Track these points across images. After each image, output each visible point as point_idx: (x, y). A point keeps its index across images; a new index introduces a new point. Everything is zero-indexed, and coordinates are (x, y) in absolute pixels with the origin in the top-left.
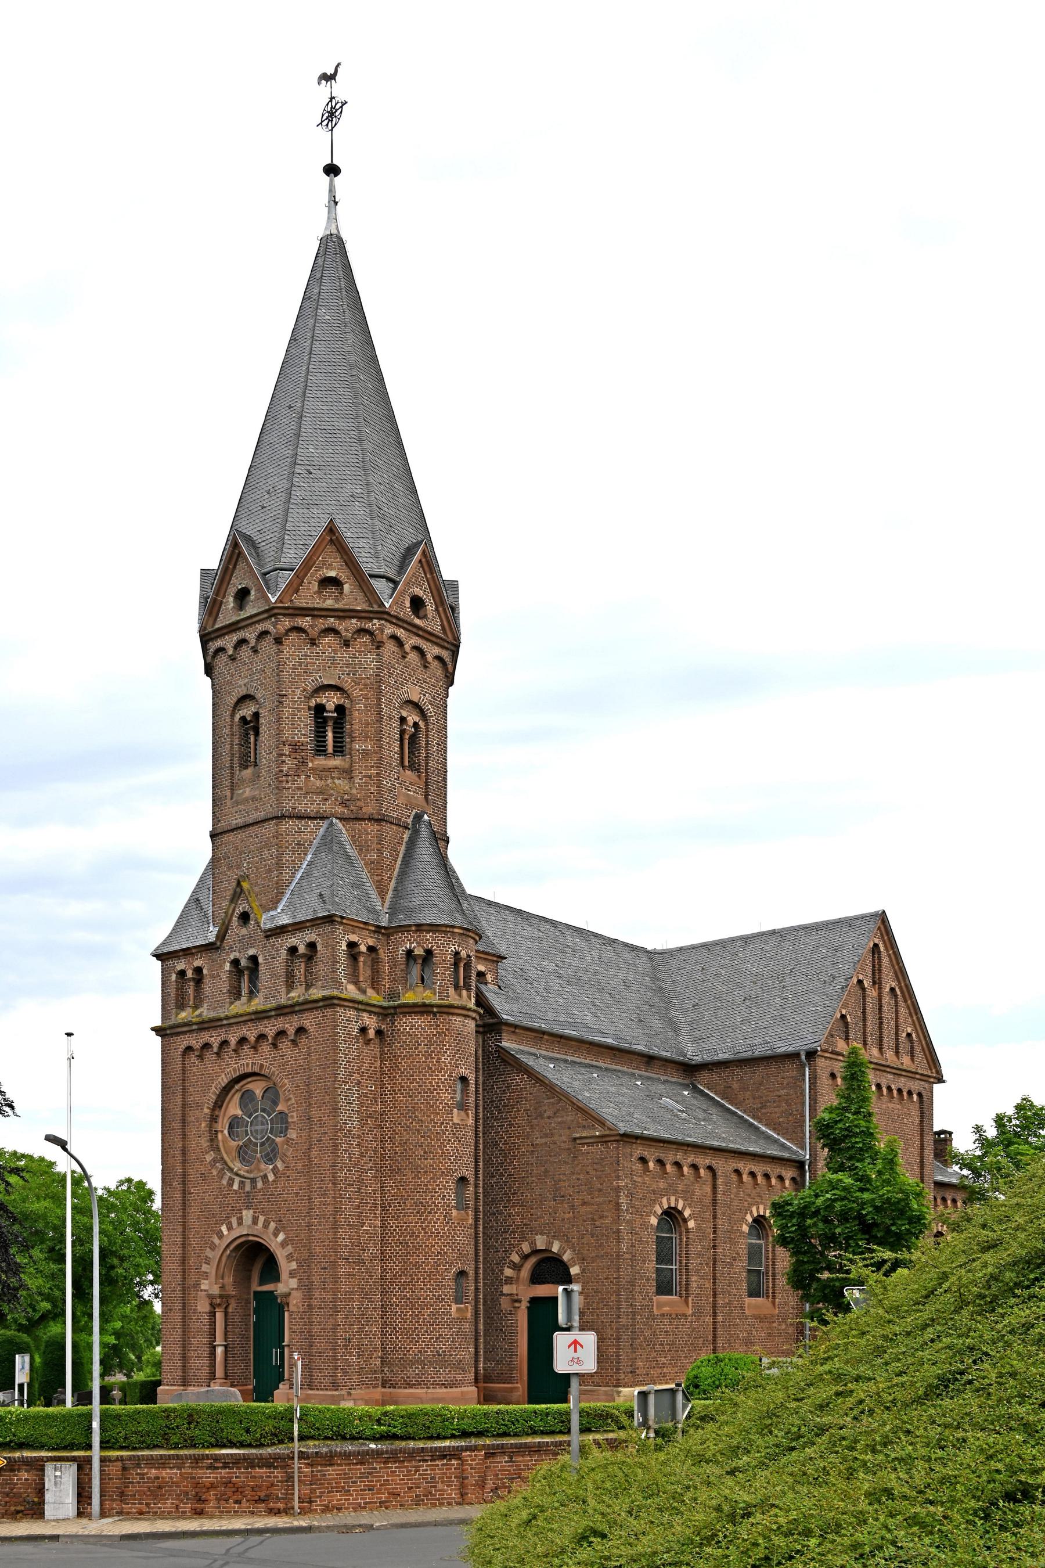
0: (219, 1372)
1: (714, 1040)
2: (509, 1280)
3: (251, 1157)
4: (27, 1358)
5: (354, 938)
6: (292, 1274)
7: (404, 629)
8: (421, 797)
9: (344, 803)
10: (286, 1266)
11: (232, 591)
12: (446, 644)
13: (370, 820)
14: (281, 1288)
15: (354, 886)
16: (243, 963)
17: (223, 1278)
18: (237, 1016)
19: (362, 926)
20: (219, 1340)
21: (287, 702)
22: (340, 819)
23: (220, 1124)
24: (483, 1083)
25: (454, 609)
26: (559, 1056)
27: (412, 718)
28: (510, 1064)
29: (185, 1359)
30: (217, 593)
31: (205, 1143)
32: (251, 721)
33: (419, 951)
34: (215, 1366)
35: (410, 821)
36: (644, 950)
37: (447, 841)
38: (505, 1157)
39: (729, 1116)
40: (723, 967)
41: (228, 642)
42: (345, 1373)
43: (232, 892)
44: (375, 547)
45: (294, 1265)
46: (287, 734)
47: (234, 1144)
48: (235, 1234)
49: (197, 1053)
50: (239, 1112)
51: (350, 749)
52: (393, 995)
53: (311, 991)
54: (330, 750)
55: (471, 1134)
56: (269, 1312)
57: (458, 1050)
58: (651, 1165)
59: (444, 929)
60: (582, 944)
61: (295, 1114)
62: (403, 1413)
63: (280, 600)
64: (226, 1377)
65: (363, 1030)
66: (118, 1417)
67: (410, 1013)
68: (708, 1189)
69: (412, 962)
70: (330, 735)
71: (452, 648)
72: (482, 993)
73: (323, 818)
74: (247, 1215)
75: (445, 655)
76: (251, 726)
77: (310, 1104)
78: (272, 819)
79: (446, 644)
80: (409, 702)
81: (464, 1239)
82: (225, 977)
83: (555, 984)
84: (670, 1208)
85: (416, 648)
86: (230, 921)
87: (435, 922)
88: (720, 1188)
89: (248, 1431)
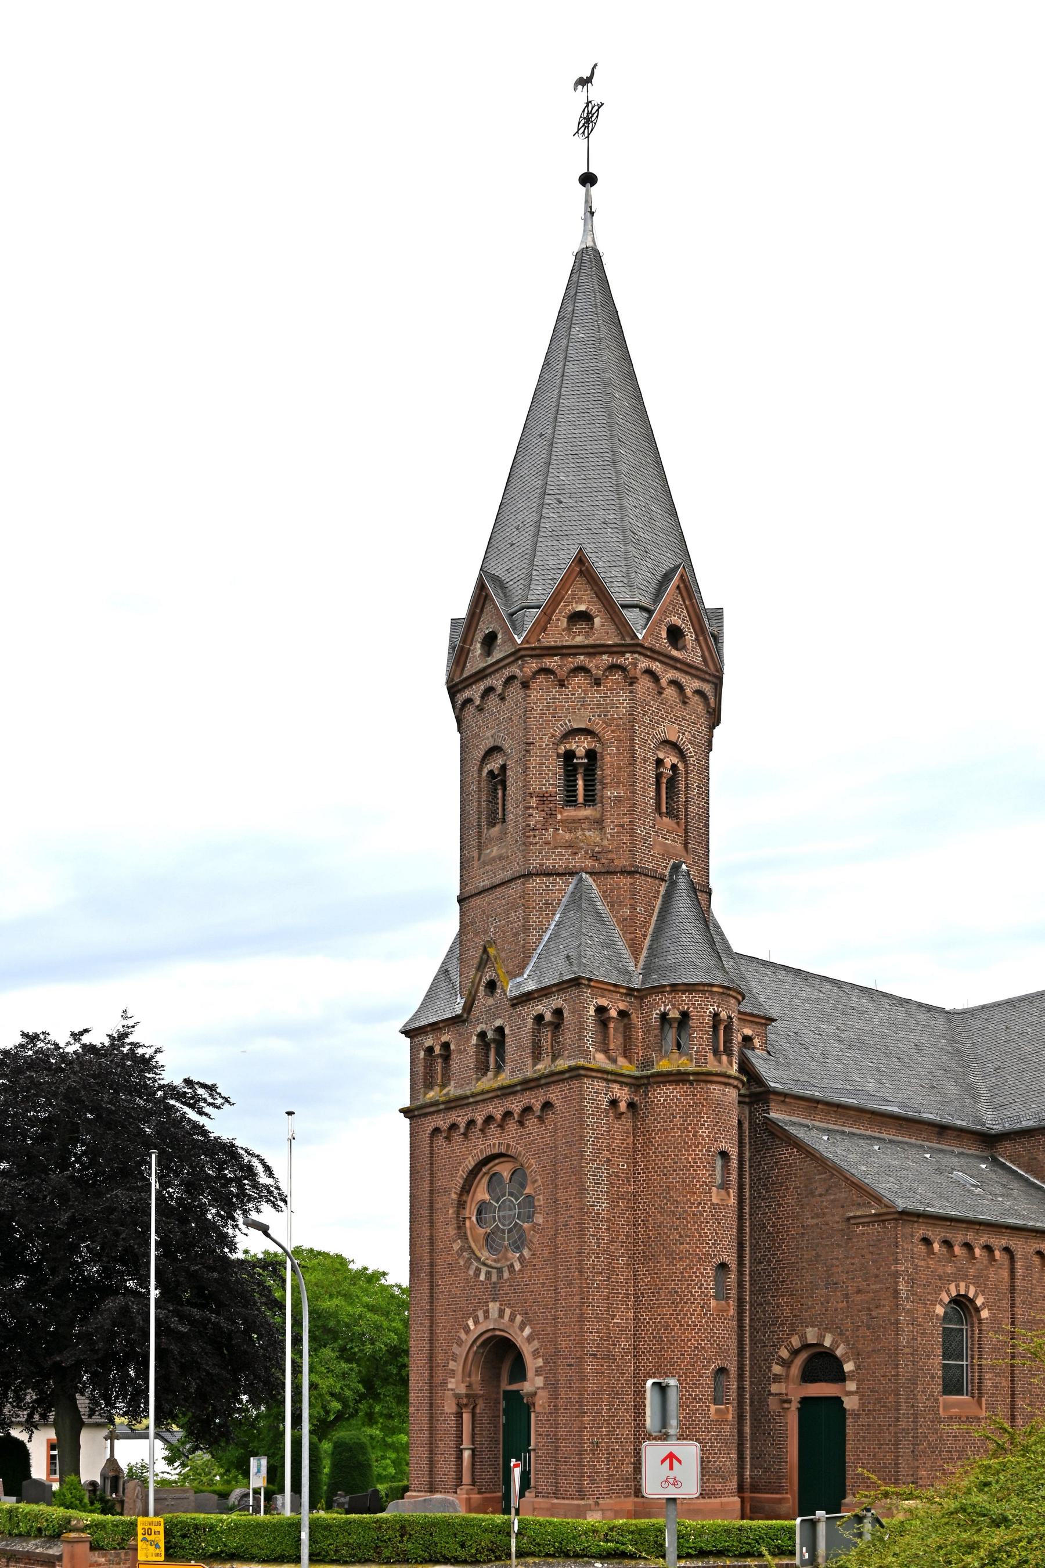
0: (466, 1478)
1: (1017, 1107)
2: (777, 1379)
3: (500, 1245)
4: (264, 1461)
5: (603, 1002)
6: (538, 1372)
7: (661, 662)
8: (680, 846)
9: (594, 857)
10: (532, 1363)
11: (479, 637)
12: (707, 677)
13: (622, 872)
14: (527, 1387)
15: (606, 945)
16: (490, 1035)
17: (470, 1377)
18: (483, 1093)
19: (612, 988)
20: (466, 1444)
21: (534, 750)
22: (591, 874)
23: (468, 1209)
24: (750, 1160)
25: (717, 638)
26: (836, 1127)
27: (670, 759)
28: (778, 1137)
29: (431, 1463)
30: (464, 640)
31: (452, 1231)
32: (498, 775)
33: (674, 1014)
34: (461, 1472)
35: (667, 872)
36: (942, 1010)
37: (709, 893)
38: (773, 1240)
39: (1033, 1192)
40: (1029, 1025)
41: (475, 692)
42: (593, 1481)
43: (478, 960)
44: (628, 574)
45: (540, 1362)
46: (535, 786)
47: (482, 1231)
48: (482, 1328)
49: (444, 1135)
50: (487, 1197)
51: (602, 797)
52: (647, 1063)
53: (557, 1062)
54: (581, 799)
55: (732, 1215)
56: (517, 1411)
57: (715, 1123)
58: (936, 1246)
59: (701, 988)
60: (869, 1005)
61: (541, 1197)
62: (633, 1528)
63: (526, 641)
64: (473, 1484)
65: (614, 1103)
66: (328, 1527)
67: (664, 1083)
68: (1006, 1274)
69: (667, 1026)
70: (580, 783)
71: (715, 680)
72: (748, 1059)
73: (572, 874)
74: (494, 1307)
75: (707, 688)
76: (498, 780)
77: (557, 1186)
78: (519, 877)
79: (707, 677)
80: (666, 742)
81: (725, 1333)
82: (472, 1051)
83: (834, 1048)
84: (959, 1295)
85: (673, 683)
86: (477, 991)
87: (690, 981)
88: (1020, 1272)
89: (463, 1546)
